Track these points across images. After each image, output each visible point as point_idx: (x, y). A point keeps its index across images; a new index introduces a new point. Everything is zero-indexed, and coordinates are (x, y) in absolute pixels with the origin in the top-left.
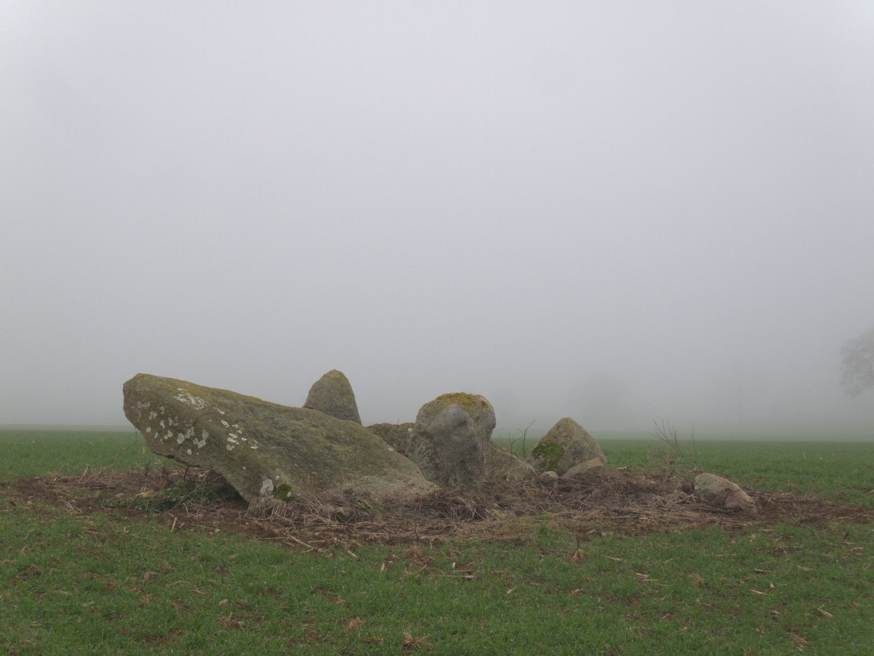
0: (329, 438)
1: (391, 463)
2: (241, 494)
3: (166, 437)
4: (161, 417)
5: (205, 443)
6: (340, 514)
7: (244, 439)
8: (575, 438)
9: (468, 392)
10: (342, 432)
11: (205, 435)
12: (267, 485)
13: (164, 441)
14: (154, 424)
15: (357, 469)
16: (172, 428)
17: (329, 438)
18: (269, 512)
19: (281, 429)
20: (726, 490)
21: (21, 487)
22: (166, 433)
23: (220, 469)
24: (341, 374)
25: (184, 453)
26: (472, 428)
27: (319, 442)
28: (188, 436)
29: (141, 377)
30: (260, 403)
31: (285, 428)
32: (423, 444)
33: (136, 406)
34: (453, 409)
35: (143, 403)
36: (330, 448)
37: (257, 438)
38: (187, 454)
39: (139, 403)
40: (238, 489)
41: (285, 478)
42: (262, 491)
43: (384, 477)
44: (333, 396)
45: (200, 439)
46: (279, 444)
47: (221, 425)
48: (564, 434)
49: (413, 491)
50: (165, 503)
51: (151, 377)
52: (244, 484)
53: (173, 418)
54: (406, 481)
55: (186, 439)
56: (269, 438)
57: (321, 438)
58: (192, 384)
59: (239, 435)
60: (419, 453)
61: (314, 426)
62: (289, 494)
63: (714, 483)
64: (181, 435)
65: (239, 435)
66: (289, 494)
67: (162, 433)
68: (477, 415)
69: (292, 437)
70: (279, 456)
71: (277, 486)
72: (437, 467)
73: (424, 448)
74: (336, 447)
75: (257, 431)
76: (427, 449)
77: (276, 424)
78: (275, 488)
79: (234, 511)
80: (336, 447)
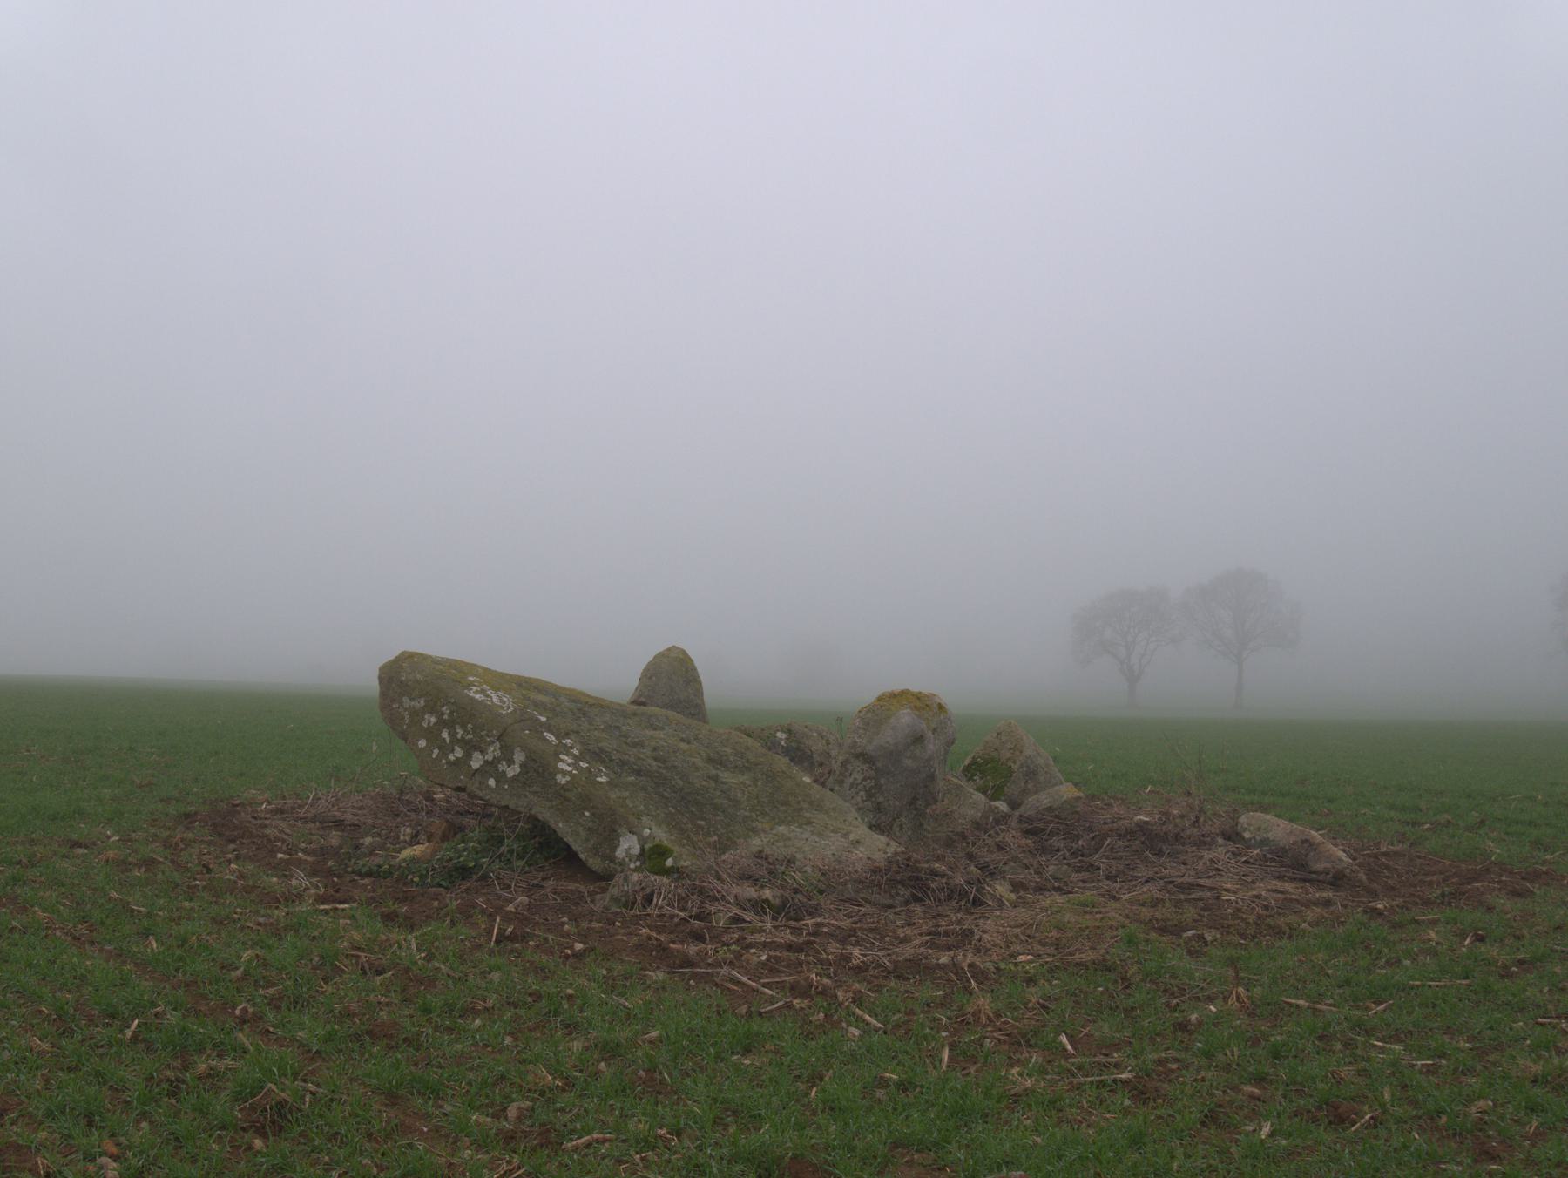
0: (710, 760)
1: (811, 803)
2: (582, 856)
3: (451, 757)
4: (442, 724)
5: (518, 770)
6: (767, 901)
7: (585, 765)
8: (1027, 752)
9: (915, 688)
10: (729, 750)
11: (519, 757)
12: (628, 845)
13: (449, 763)
14: (432, 735)
15: (763, 813)
16: (463, 743)
17: (710, 760)
18: (649, 900)
19: (635, 745)
20: (1303, 842)
21: (214, 825)
22: (453, 751)
23: (544, 813)
24: (684, 653)
25: (483, 784)
26: (932, 746)
27: (697, 769)
28: (489, 757)
29: (407, 658)
30: (591, 701)
31: (640, 744)
32: (858, 772)
33: (401, 704)
34: (905, 718)
35: (412, 699)
36: (716, 779)
37: (603, 762)
38: (488, 787)
39: (406, 700)
40: (575, 847)
41: (662, 836)
42: (620, 853)
43: (809, 828)
44: (672, 680)
45: (511, 762)
46: (638, 773)
47: (545, 739)
48: (1009, 745)
49: (861, 852)
50: (456, 869)
51: (424, 657)
52: (587, 840)
53: (463, 726)
54: (846, 835)
55: (486, 762)
56: (623, 763)
57: (700, 763)
58: (486, 670)
59: (575, 756)
60: (852, 786)
61: (683, 740)
62: (669, 862)
63: (1279, 829)
64: (476, 754)
65: (575, 756)
66: (669, 862)
67: (445, 749)
68: (933, 725)
69: (656, 759)
70: (643, 794)
71: (647, 847)
72: (878, 808)
73: (860, 778)
74: (725, 776)
75: (601, 750)
76: (864, 779)
77: (626, 736)
78: (643, 849)
79: (572, 886)
80: (725, 776)
